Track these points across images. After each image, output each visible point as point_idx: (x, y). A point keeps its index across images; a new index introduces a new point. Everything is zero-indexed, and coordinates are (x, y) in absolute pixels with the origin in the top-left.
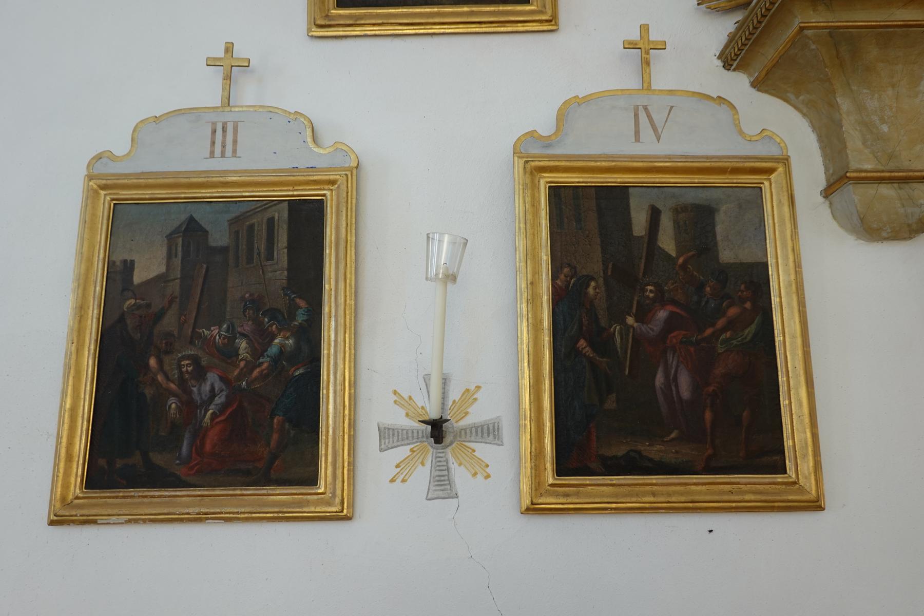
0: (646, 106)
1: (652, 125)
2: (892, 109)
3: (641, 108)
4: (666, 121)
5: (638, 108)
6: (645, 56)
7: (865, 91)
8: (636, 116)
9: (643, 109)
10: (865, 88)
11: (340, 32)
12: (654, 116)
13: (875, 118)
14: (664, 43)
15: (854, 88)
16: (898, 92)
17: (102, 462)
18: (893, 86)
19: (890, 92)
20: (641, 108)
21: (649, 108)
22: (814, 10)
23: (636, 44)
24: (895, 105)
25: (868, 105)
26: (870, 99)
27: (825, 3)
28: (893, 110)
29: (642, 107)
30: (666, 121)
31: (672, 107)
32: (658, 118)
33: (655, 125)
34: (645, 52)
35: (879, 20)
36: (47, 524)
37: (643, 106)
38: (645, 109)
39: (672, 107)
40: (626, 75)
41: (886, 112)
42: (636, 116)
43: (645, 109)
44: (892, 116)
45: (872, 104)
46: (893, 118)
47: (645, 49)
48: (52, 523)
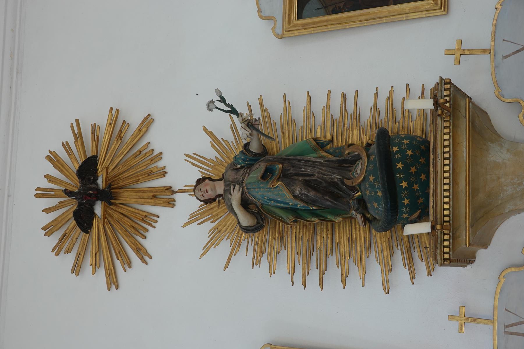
0: (505, 326)
1: (518, 325)
2: (513, 178)
3: (506, 330)
4: (516, 315)
5: (506, 331)
6: (470, 321)
7: (501, 195)
8: (512, 333)
9: (507, 328)
10: (500, 195)
11: (47, 197)
12: (512, 322)
13: (519, 189)
14: (461, 307)
15: (500, 202)
16: (503, 175)
17: (41, 194)
18: (499, 178)
19: (502, 180)
20: (506, 330)
21: (506, 324)
22: (459, 237)
23: (462, 325)
24: (510, 176)
25: (510, 193)
26: (506, 191)
27: (456, 232)
28: (513, 177)
29: (505, 329)
30: (516, 315)
31: (506, 310)
32: (513, 320)
33: (519, 322)
34: (467, 320)
35: (465, 199)
36: (150, 113)
37: (505, 328)
38: (507, 327)
39: (506, 310)
40: (476, 327)
41: (515, 182)
42: (512, 333)
43: (507, 327)
44: (518, 178)
45: (509, 190)
46: (519, 178)
47: (465, 320)
48: (167, 173)
